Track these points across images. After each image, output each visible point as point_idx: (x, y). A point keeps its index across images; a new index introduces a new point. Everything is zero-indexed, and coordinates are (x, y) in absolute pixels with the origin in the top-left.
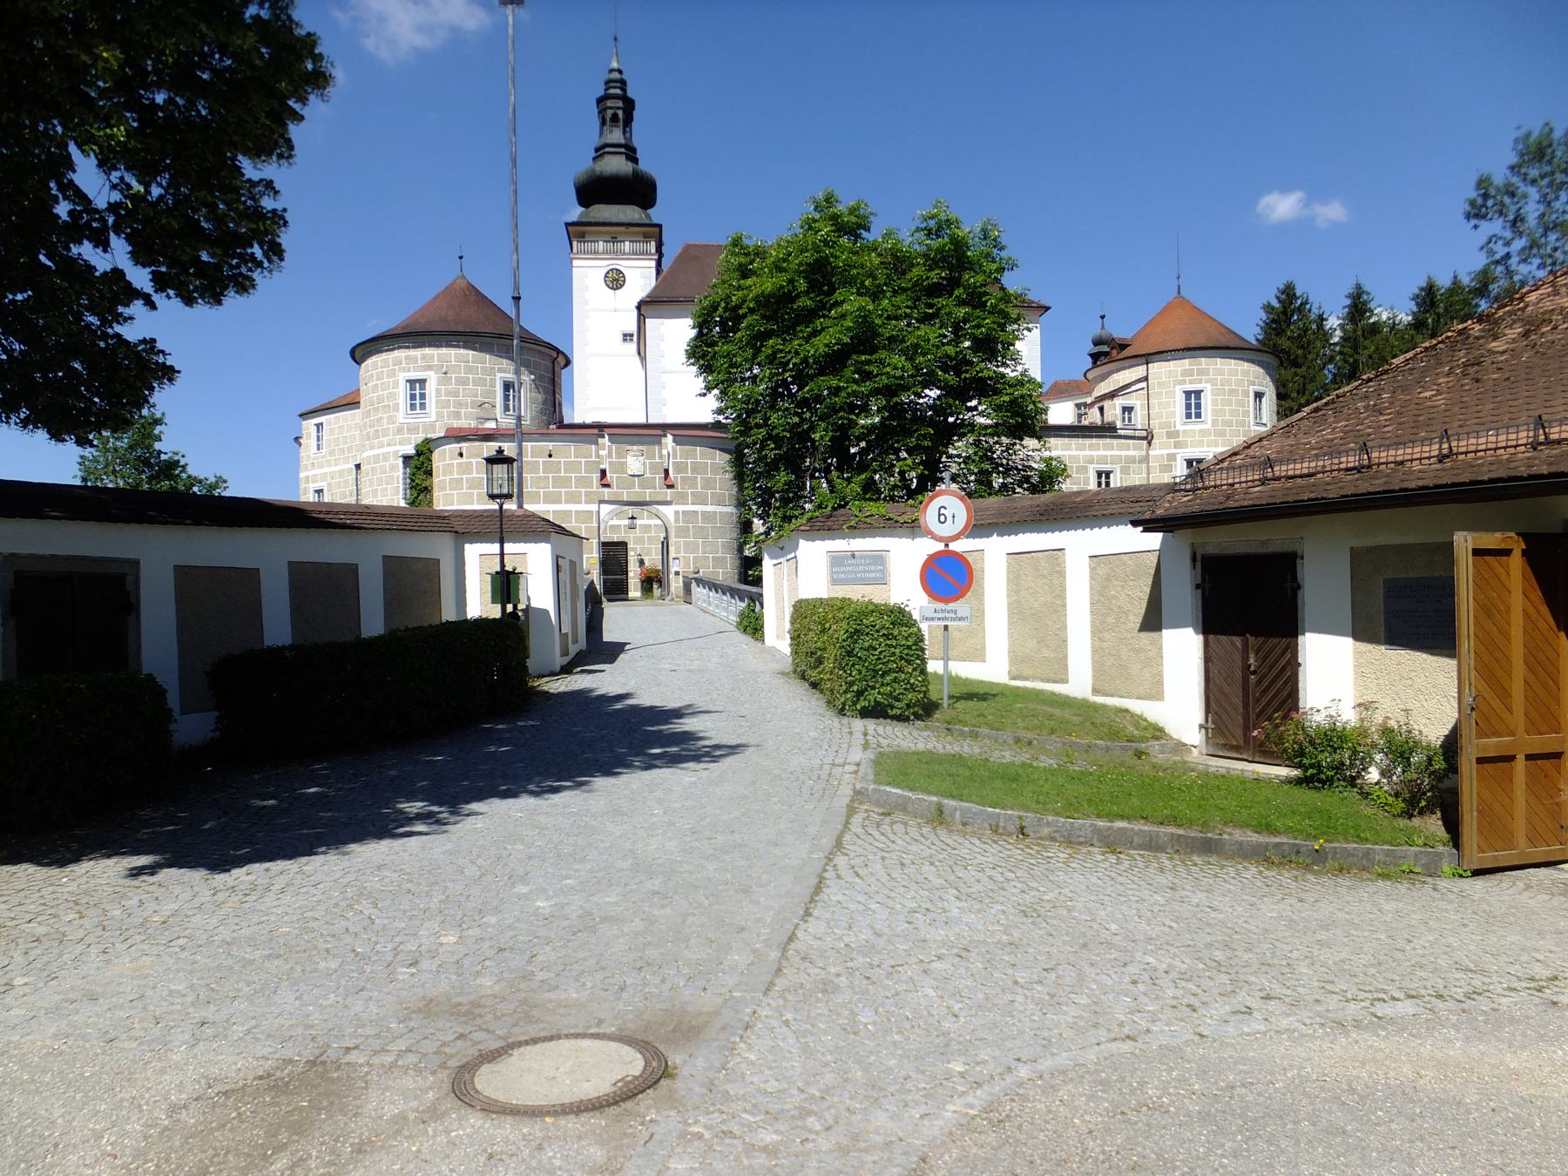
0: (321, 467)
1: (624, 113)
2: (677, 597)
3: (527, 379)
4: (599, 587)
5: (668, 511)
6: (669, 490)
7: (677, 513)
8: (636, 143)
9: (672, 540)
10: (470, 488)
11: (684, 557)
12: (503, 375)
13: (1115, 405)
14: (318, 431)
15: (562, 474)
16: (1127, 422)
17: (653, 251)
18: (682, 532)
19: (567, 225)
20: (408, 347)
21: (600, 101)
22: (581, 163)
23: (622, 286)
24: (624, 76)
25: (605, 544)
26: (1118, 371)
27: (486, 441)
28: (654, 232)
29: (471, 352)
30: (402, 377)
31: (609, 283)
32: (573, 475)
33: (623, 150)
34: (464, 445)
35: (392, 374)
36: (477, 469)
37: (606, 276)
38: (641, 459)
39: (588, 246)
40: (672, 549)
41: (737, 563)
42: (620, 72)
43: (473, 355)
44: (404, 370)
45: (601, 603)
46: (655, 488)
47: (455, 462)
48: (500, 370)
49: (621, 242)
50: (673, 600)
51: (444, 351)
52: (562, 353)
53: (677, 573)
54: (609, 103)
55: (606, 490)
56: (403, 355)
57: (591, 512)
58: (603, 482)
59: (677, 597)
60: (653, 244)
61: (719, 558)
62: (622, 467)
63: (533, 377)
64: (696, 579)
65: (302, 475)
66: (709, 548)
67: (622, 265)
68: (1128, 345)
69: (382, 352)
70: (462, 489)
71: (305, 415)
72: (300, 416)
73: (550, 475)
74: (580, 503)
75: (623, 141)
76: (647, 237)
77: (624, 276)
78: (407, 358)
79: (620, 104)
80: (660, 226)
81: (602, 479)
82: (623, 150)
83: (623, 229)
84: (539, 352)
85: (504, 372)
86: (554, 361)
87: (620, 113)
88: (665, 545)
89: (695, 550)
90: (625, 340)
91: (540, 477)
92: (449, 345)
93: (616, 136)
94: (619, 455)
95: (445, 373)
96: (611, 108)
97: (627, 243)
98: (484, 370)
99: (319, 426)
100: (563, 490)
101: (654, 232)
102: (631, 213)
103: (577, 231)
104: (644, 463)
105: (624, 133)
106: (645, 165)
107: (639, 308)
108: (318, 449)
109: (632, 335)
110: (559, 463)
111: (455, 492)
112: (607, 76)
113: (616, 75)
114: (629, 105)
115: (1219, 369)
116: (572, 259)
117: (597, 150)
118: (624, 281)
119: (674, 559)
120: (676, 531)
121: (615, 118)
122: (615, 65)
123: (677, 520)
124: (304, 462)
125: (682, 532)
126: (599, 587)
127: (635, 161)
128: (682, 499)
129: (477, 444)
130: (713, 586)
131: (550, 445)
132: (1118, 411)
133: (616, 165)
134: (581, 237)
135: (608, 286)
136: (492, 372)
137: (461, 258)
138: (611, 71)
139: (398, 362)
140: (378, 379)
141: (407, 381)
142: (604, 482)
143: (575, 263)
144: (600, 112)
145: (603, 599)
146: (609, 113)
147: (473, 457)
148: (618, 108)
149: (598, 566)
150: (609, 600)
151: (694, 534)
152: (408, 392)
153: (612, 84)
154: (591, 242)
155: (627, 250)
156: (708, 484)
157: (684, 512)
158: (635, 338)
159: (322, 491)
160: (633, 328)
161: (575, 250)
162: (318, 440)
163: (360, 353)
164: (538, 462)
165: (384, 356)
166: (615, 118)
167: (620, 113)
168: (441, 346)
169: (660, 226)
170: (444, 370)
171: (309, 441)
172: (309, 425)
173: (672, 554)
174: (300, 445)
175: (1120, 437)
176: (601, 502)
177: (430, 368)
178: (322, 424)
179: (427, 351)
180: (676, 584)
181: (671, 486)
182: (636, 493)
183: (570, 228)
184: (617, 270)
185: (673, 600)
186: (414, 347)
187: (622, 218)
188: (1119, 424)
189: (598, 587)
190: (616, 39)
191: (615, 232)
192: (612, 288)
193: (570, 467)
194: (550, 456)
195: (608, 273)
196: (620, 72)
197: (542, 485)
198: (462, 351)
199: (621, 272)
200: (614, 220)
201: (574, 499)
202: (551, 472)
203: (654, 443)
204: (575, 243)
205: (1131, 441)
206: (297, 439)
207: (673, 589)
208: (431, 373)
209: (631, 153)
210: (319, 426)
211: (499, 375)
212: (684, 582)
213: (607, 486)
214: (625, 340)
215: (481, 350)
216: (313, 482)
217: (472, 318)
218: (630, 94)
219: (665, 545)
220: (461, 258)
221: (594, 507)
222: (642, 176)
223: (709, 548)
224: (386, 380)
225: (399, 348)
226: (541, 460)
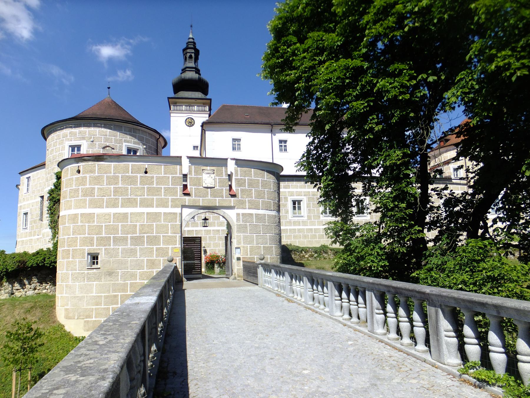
0: (28, 200)
1: (195, 55)
2: (239, 276)
3: (141, 147)
4: (180, 270)
5: (232, 214)
6: (232, 199)
7: (238, 215)
8: (199, 68)
9: (235, 234)
10: (84, 195)
11: (244, 247)
12: (127, 144)
13: (449, 167)
14: (28, 182)
15: (155, 186)
16: (456, 177)
17: (207, 110)
18: (242, 228)
19: (169, 98)
20: (71, 127)
21: (184, 50)
22: (176, 75)
23: (193, 125)
24: (195, 41)
25: (184, 238)
26: (446, 151)
27: (98, 161)
28: (209, 103)
29: (108, 130)
30: (67, 144)
31: (187, 124)
32: (163, 187)
33: (194, 70)
34: (82, 165)
35: (62, 143)
36: (90, 182)
37: (186, 121)
38: (213, 176)
39: (178, 108)
40: (234, 241)
41: (279, 251)
42: (193, 39)
43: (110, 132)
44: (68, 140)
45: (181, 282)
46: (222, 197)
47: (74, 177)
48: (125, 141)
49: (193, 106)
50: (235, 279)
51: (92, 129)
52: (163, 137)
53: (238, 259)
54: (188, 51)
55: (187, 198)
56: (69, 131)
57: (175, 214)
58: (185, 192)
59: (239, 276)
60: (207, 107)
61: (268, 247)
62: (199, 182)
63: (145, 146)
64: (263, 265)
65: (19, 205)
66: (260, 241)
67: (193, 116)
68: (449, 140)
69: (57, 131)
70: (78, 196)
71: (22, 173)
72: (19, 173)
73: (146, 186)
74: (168, 207)
75: (194, 66)
76: (204, 105)
77: (194, 121)
78: (70, 133)
79: (193, 51)
80: (210, 100)
81: (184, 190)
82: (194, 70)
83: (193, 101)
84: (149, 134)
85: (128, 142)
86: (157, 140)
87: (193, 55)
88: (228, 238)
89: (251, 242)
90: (194, 149)
91: (138, 188)
92: (95, 126)
93: (192, 64)
94: (196, 172)
95: (92, 142)
96: (189, 53)
97: (196, 107)
98: (116, 141)
99: (28, 178)
100: (155, 197)
101: (209, 103)
102: (199, 95)
103: (173, 102)
104: (215, 179)
105: (195, 63)
106: (204, 76)
107: (202, 126)
108: (28, 191)
109: (197, 147)
110: (153, 177)
111: (73, 199)
112: (187, 41)
113: (191, 40)
114: (197, 52)
115: (129, 177)
116: (170, 113)
117: (182, 70)
118: (194, 123)
119: (236, 248)
120: (238, 228)
121: (191, 57)
122: (191, 36)
123: (238, 220)
124: (20, 198)
125: (242, 228)
126: (180, 270)
127: (200, 74)
128: (241, 204)
129: (90, 163)
130: (267, 268)
131: (146, 165)
132: (452, 170)
133: (191, 75)
134: (175, 104)
135: (187, 125)
136: (120, 142)
137: (109, 88)
138: (190, 38)
139: (65, 136)
140: (54, 146)
141: (70, 146)
142: (185, 192)
143: (172, 115)
144: (184, 55)
145: (184, 279)
146: (188, 55)
147: (87, 172)
148: (192, 53)
149: (180, 254)
150: (189, 279)
151: (250, 230)
152: (70, 152)
153: (189, 44)
154: (179, 106)
155: (196, 110)
156: (260, 195)
157: (243, 214)
158: (199, 148)
159: (27, 213)
160: (198, 144)
161: (172, 109)
162: (28, 186)
163: (46, 132)
164: (137, 177)
165: (58, 133)
166: (191, 57)
167: (193, 55)
168: (91, 127)
169: (210, 100)
170: (92, 140)
171: (23, 188)
172: (24, 178)
173: (235, 244)
174: (19, 189)
175: (454, 184)
176: (183, 206)
177: (83, 138)
178: (30, 177)
179: (82, 129)
180: (237, 267)
181: (234, 196)
182: (208, 200)
183: (170, 100)
184: (191, 118)
185: (235, 279)
186: (75, 127)
187: (193, 96)
188: (453, 177)
189: (180, 270)
190: (191, 26)
191: (190, 102)
192: (189, 126)
193: (160, 180)
194: (146, 172)
195: (187, 119)
196: (193, 39)
197: (139, 193)
198: (103, 129)
199: (193, 119)
200: (190, 97)
201: (163, 204)
202: (146, 184)
203: (222, 166)
204: (172, 107)
205: (459, 186)
206: (17, 186)
207: (235, 271)
208: (84, 142)
209: (197, 71)
210: (28, 178)
211: (124, 144)
212: (243, 265)
213: (188, 194)
214: (194, 149)
215: (115, 130)
216: (23, 209)
217: (112, 113)
218: (197, 47)
219: (228, 238)
220: (109, 88)
221: (178, 210)
222: (205, 82)
223: (260, 241)
224: (58, 146)
225: (66, 128)
226: (139, 175)
